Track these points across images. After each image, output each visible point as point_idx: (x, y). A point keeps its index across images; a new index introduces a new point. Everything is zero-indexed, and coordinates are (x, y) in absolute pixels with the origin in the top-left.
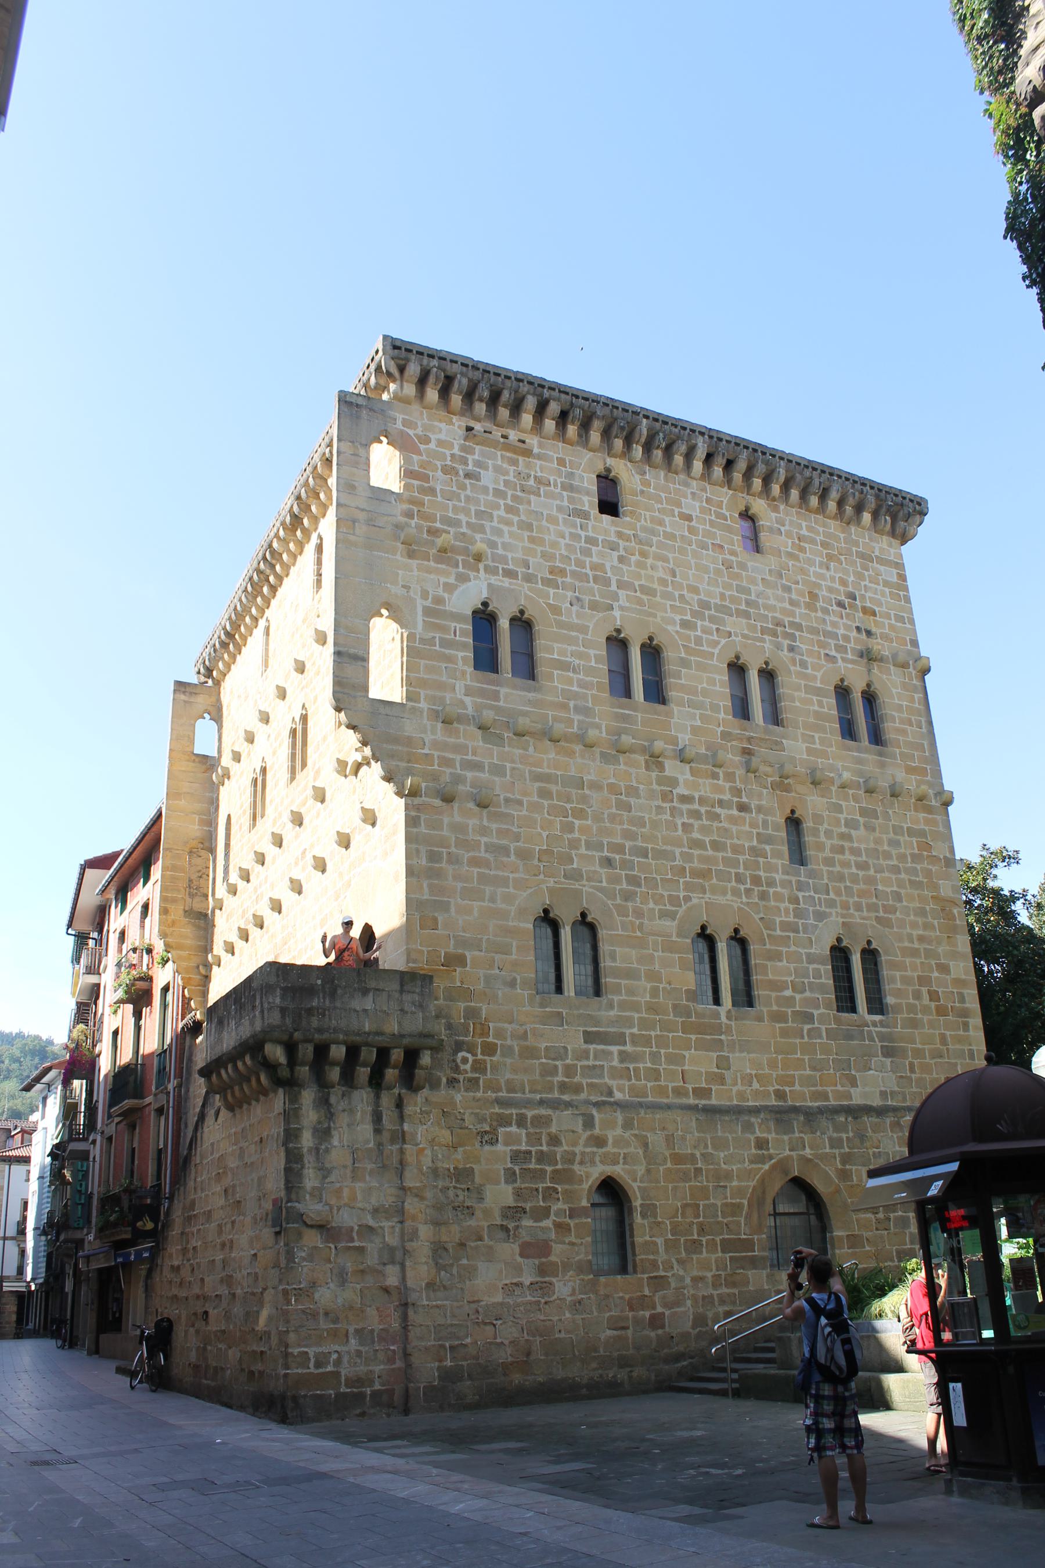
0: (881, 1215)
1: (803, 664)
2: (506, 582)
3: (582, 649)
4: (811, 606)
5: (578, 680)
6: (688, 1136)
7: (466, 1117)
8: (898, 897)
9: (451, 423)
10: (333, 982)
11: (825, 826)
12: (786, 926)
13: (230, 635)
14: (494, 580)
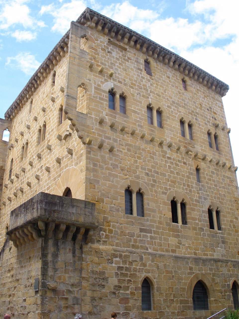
0: (223, 294)
1: (199, 124)
2: (119, 84)
3: (140, 108)
4: (201, 109)
5: (139, 117)
6: (170, 265)
7: (103, 254)
8: (224, 195)
9: (104, 37)
10: (62, 202)
11: (206, 172)
12: (196, 201)
13: (18, 104)
14: (115, 83)
